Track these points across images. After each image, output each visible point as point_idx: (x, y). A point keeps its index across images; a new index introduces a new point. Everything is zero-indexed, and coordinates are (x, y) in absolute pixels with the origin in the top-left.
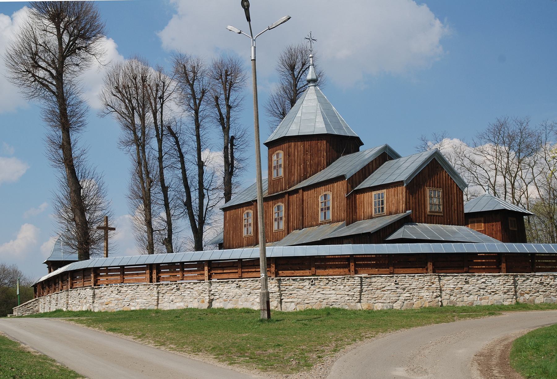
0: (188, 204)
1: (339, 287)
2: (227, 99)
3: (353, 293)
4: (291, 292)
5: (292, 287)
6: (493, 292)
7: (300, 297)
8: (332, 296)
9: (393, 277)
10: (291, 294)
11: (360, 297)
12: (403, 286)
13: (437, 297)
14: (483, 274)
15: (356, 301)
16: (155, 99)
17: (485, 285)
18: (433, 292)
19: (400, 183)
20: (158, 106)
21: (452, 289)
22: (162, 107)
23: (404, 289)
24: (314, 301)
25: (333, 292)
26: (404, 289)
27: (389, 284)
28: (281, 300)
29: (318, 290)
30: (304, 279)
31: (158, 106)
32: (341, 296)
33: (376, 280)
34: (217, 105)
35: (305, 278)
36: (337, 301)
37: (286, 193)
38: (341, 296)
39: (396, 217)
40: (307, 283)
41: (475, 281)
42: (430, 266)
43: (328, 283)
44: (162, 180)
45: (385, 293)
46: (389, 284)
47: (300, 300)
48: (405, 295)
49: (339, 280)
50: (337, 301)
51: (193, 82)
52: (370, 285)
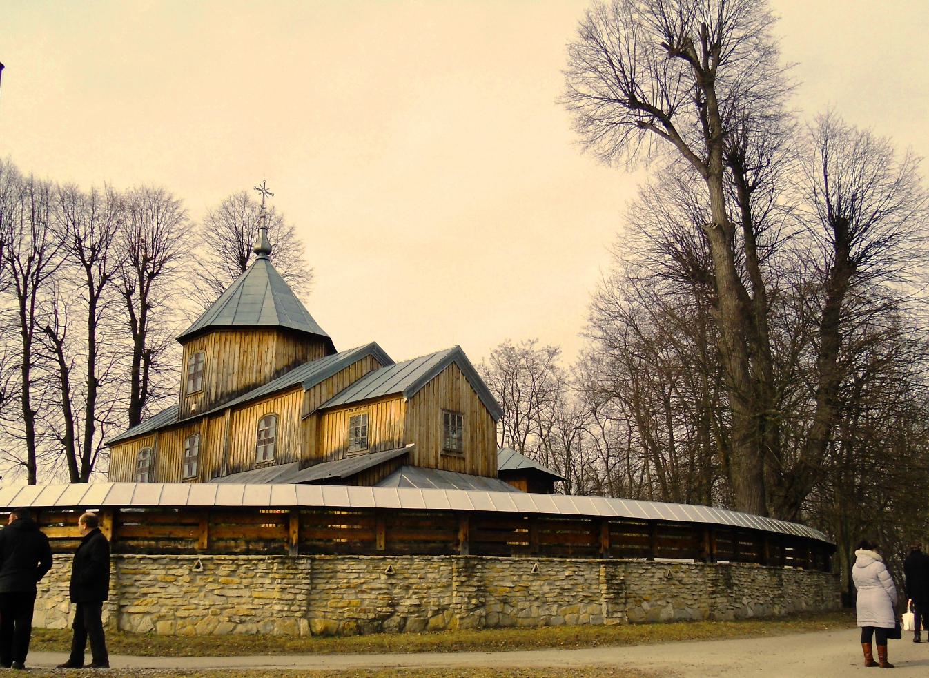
0: (69, 441)
1: (260, 581)
2: (144, 295)
3: (291, 596)
4: (144, 590)
5: (151, 577)
6: (586, 597)
7: (168, 602)
8: (243, 600)
9: (384, 559)
10: (145, 594)
11: (309, 605)
12: (406, 583)
13: (477, 607)
14: (568, 560)
15: (298, 614)
16: (25, 278)
17: (572, 582)
18: (470, 598)
19: (398, 395)
20: (30, 290)
21: (508, 589)
22: (34, 293)
23: (407, 588)
24: (201, 612)
25: (246, 593)
26: (407, 588)
27: (374, 576)
28: (121, 607)
29: (209, 587)
30: (178, 560)
31: (30, 290)
32: (263, 601)
33: (345, 566)
34: (130, 306)
35: (180, 557)
36: (253, 612)
37: (205, 416)
38: (263, 601)
39: (389, 454)
40: (184, 570)
41: (553, 573)
42: (524, 483)
43: (234, 571)
44: (26, 398)
45: (365, 596)
46: (374, 576)
47: (164, 610)
48: (409, 602)
49: (262, 566)
50: (253, 612)
51: (92, 263)
52: (331, 578)
